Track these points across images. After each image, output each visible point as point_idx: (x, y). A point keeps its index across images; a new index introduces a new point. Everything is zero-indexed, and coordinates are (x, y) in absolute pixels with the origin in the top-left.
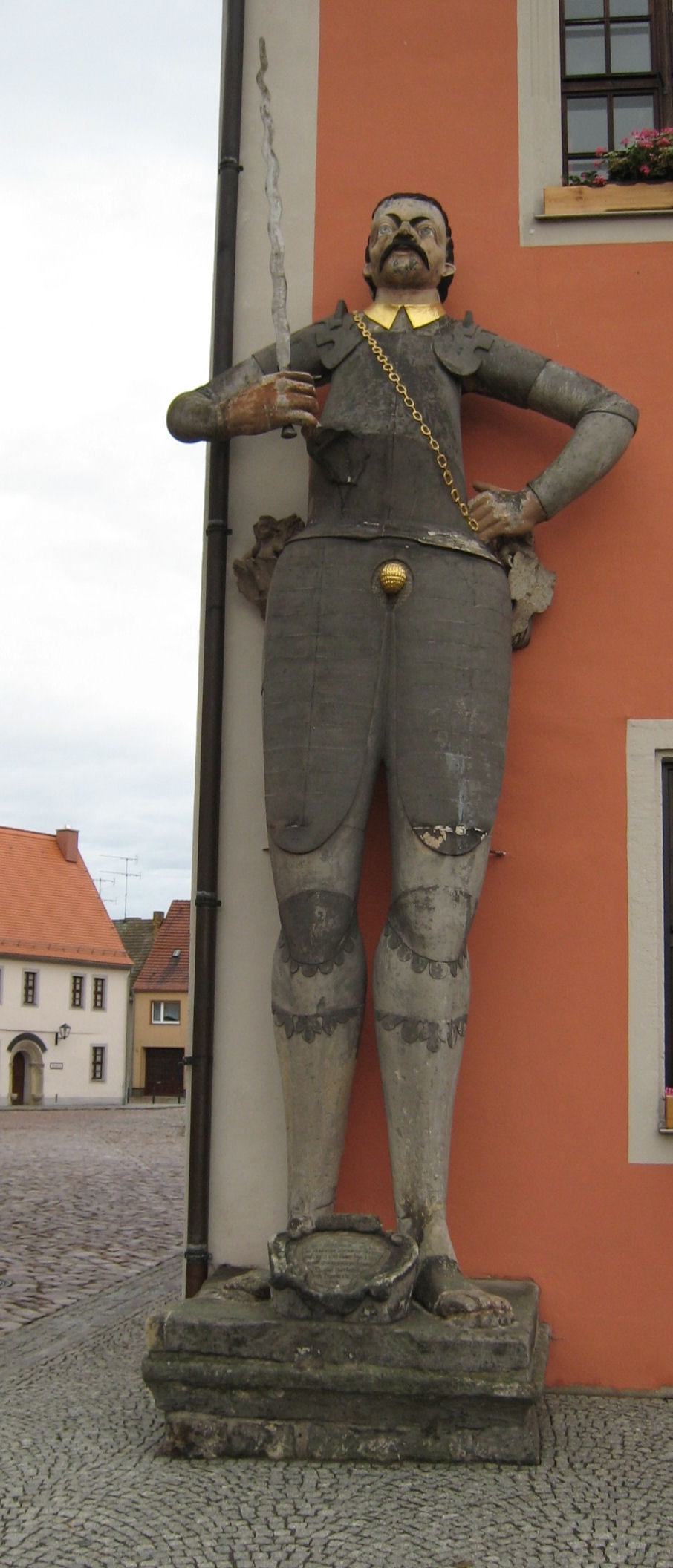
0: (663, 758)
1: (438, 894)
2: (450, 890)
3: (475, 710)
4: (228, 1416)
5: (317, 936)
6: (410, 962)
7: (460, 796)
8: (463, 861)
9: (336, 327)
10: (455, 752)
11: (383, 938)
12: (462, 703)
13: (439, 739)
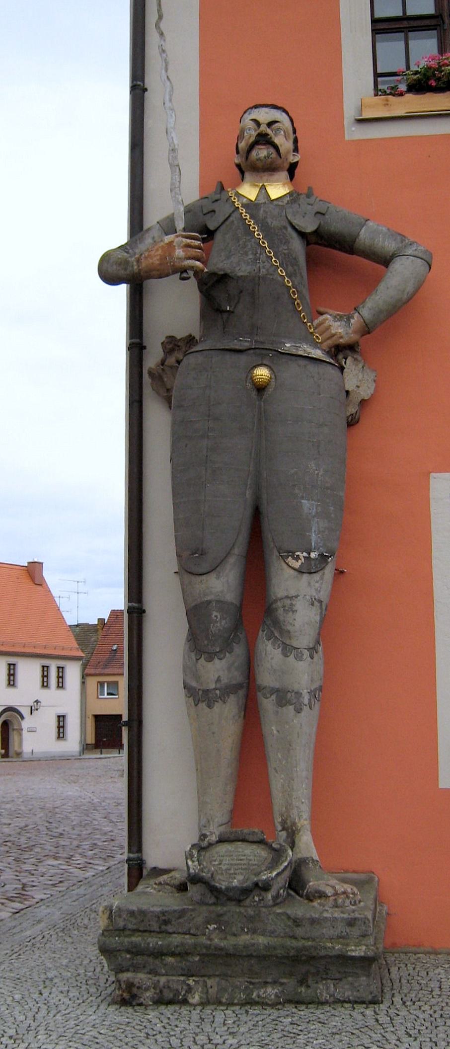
1: (299, 600)
3: (321, 470)
6: (280, 649)
7: (313, 531)
8: (317, 577)
9: (217, 201)
10: (308, 500)
11: (261, 632)
12: (312, 465)
13: (297, 491)
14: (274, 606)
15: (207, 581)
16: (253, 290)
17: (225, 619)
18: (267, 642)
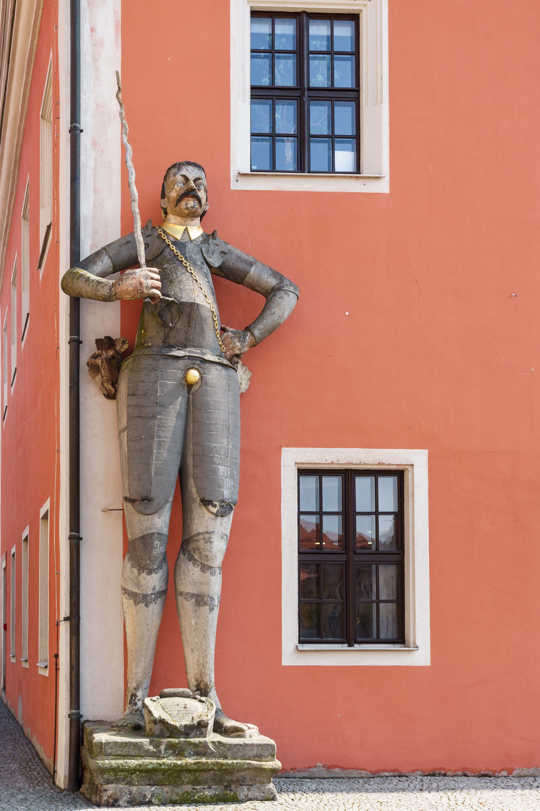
2: (220, 533)
4: (133, 785)
6: (199, 568)
8: (225, 519)
9: (149, 236)
17: (162, 546)
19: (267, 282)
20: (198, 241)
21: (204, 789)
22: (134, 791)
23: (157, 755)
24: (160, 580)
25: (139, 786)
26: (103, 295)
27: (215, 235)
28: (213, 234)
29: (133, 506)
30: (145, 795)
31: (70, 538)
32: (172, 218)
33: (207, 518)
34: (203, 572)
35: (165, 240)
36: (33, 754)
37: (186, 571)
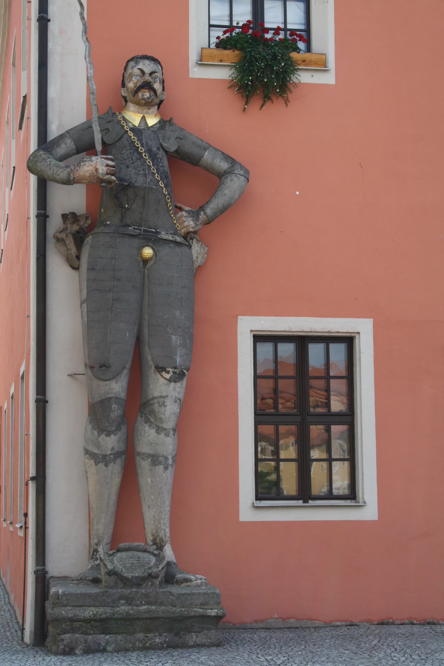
0: (254, 334)
1: (168, 399)
2: (173, 397)
3: (183, 316)
5: (113, 418)
6: (155, 430)
7: (178, 355)
8: (178, 384)
9: (110, 122)
10: (175, 335)
11: (139, 418)
12: (178, 313)
13: (168, 330)
14: (151, 402)
15: (110, 385)
16: (144, 196)
17: (120, 409)
18: (145, 425)
19: (220, 166)
20: (155, 128)
21: (155, 636)
22: (89, 640)
23: (111, 605)
24: (118, 442)
25: (94, 635)
26: (62, 179)
27: (171, 122)
28: (170, 120)
29: (92, 373)
30: (100, 643)
31: (37, 401)
32: (131, 106)
33: (161, 384)
34: (158, 433)
35: (124, 126)
36: (13, 618)
37: (143, 432)
